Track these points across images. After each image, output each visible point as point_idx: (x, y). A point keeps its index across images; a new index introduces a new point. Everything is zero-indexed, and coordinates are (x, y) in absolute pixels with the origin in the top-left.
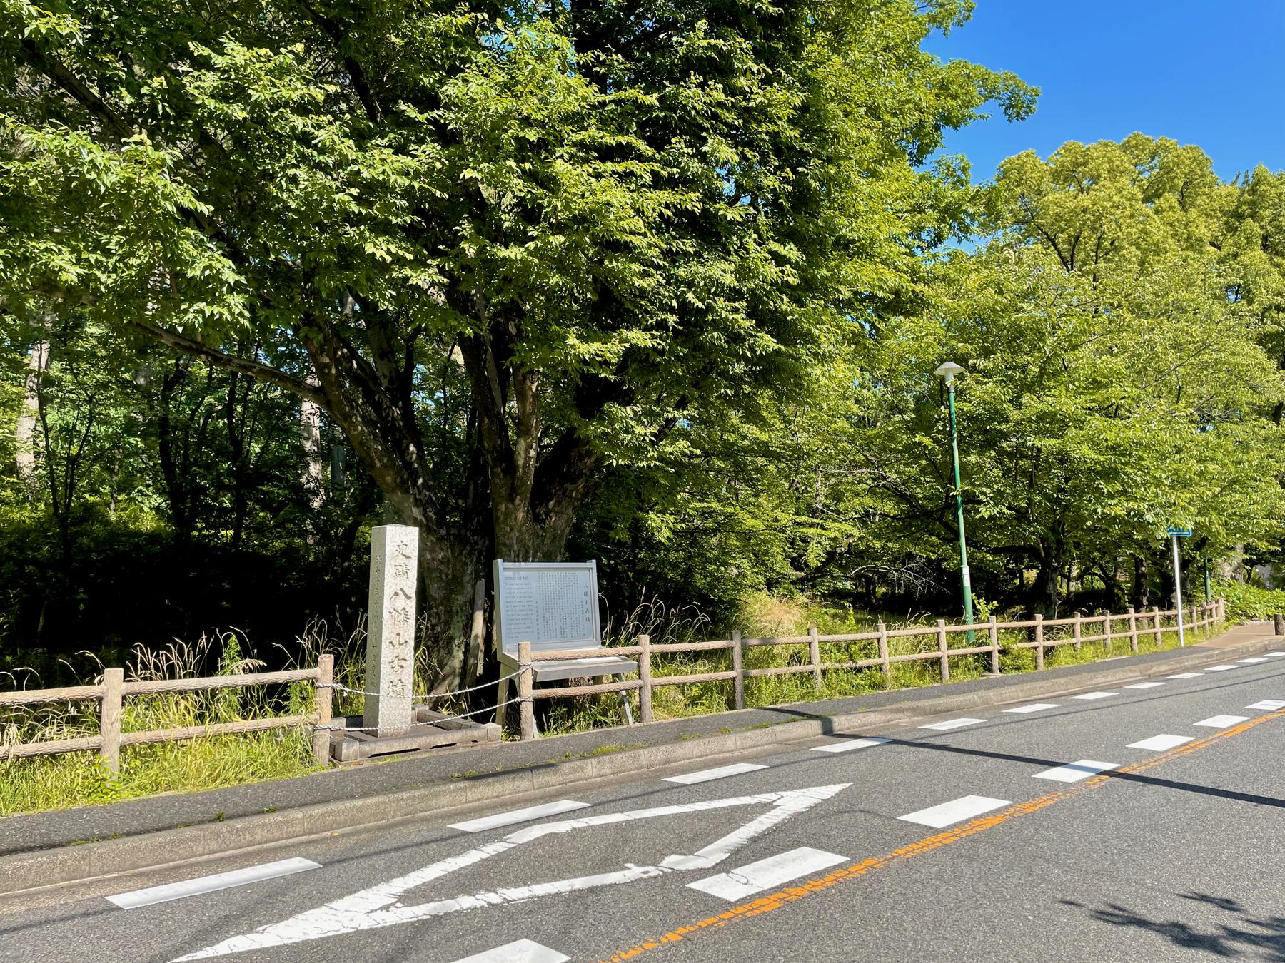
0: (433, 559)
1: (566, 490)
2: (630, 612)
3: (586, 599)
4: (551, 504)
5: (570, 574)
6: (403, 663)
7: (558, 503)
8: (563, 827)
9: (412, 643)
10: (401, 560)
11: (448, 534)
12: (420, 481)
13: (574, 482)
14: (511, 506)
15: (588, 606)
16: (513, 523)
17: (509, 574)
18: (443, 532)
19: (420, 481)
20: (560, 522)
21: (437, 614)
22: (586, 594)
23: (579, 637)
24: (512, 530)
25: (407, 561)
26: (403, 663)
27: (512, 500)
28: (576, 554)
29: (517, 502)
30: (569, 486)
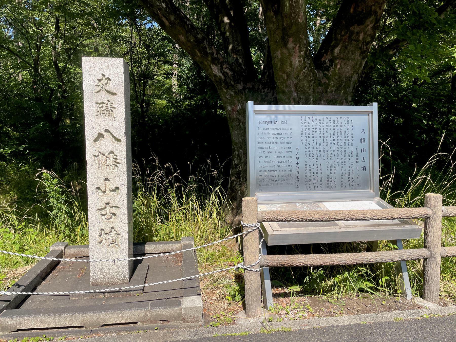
0: (233, 110)
1: (352, 33)
2: (421, 165)
3: (361, 146)
4: (337, 50)
5: (342, 119)
6: (115, 210)
7: (345, 48)
8: (395, 228)
9: (124, 190)
10: (104, 97)
11: (244, 88)
12: (231, 47)
13: (361, 22)
14: (285, 51)
15: (366, 155)
16: (288, 69)
17: (262, 117)
18: (240, 87)
19: (231, 47)
20: (347, 67)
21: (238, 155)
22: (363, 141)
23: (351, 185)
24: (288, 76)
25: (111, 98)
26: (115, 210)
27: (285, 44)
28: (359, 99)
29: (291, 45)
30: (355, 28)
